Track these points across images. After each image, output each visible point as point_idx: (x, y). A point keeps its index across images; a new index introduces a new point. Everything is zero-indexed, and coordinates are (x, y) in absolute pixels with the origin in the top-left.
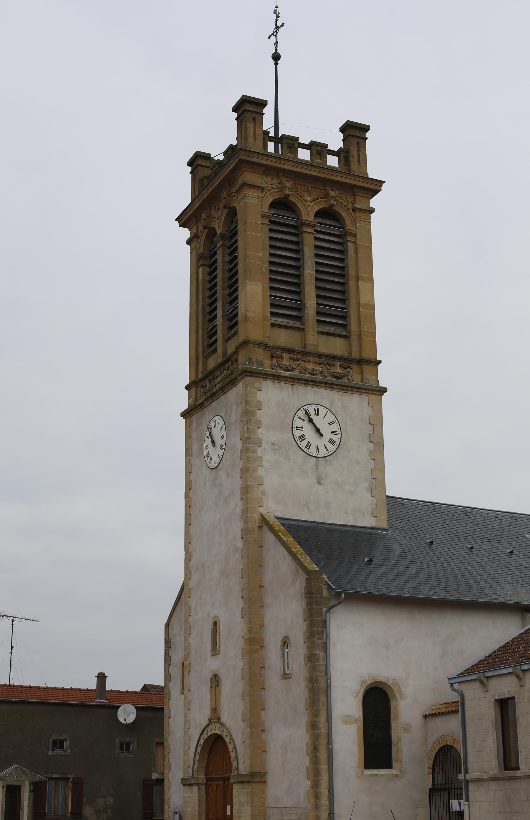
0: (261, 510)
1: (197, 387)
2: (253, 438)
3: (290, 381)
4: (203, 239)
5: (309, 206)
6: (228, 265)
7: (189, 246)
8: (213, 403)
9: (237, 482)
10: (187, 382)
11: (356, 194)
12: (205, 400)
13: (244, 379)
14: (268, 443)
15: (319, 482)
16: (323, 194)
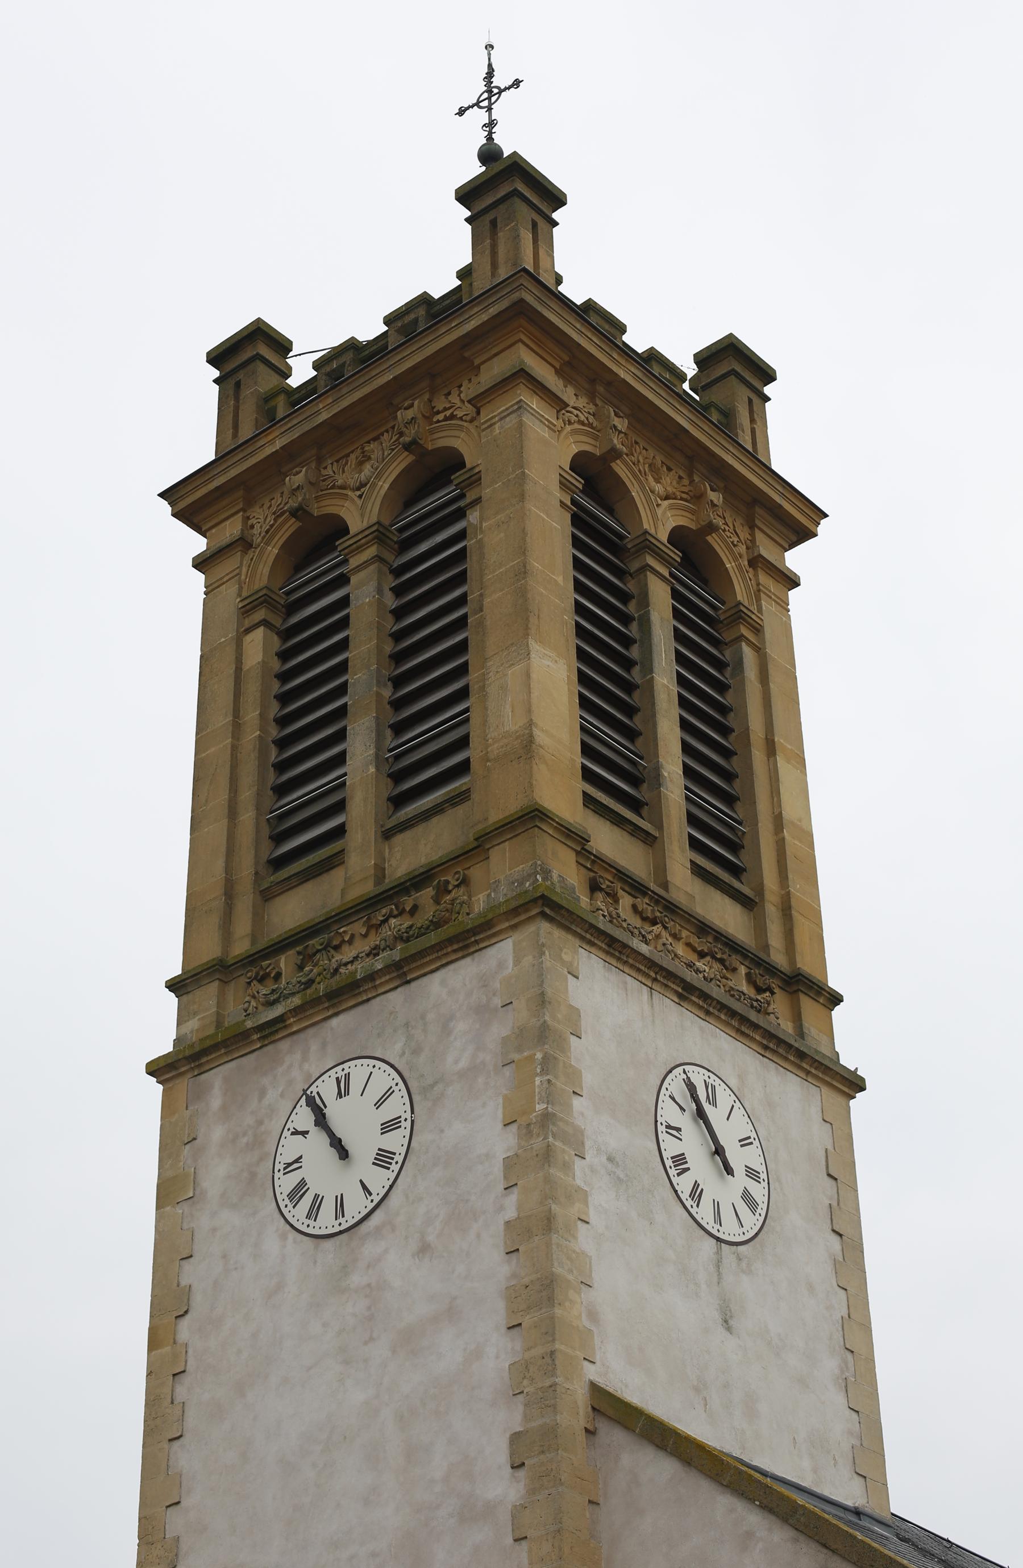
0: (592, 1373)
1: (224, 982)
2: (561, 1119)
3: (647, 976)
4: (273, 551)
5: (658, 505)
6: (390, 618)
7: (200, 578)
8: (335, 1022)
9: (486, 1266)
10: (176, 970)
11: (758, 522)
12: (296, 1011)
13: (531, 928)
14: (599, 1150)
15: (726, 1321)
16: (685, 489)
